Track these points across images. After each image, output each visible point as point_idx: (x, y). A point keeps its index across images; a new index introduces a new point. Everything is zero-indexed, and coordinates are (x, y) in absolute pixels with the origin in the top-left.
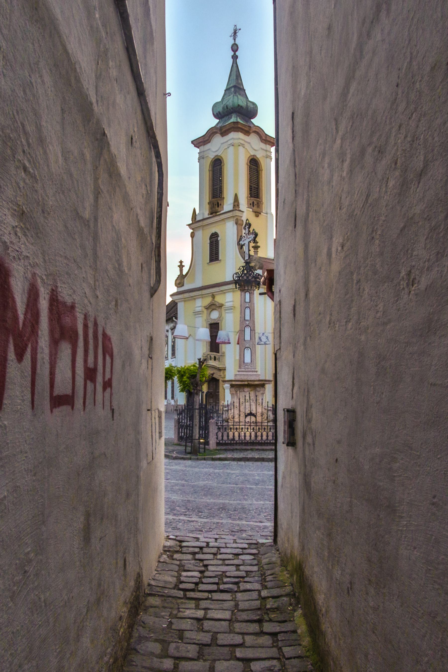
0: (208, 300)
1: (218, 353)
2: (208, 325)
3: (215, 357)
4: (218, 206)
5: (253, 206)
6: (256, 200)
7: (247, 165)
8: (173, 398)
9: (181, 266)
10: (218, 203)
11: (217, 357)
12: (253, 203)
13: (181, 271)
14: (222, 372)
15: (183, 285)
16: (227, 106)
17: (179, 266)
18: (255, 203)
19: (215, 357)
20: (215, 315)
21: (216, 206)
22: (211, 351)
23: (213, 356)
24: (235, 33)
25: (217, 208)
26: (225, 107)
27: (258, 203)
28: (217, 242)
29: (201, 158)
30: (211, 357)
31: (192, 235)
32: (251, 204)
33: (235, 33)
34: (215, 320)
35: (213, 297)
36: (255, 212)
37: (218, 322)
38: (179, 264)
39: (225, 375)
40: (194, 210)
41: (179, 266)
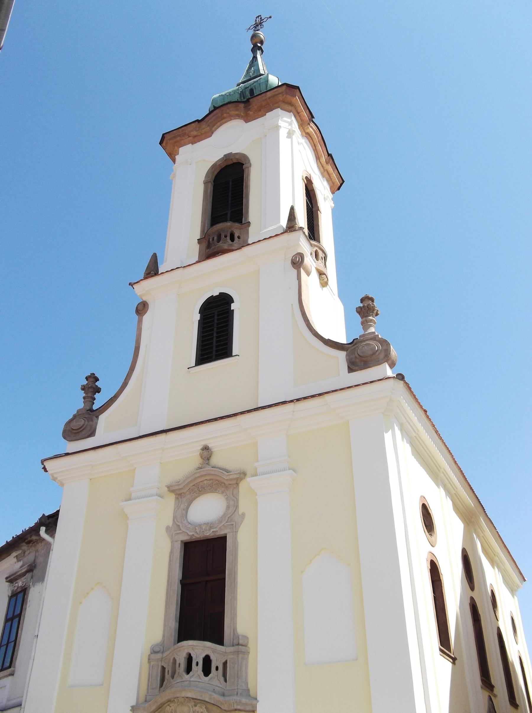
2: (178, 547)
3: (207, 661)
9: (92, 387)
13: (90, 398)
15: (92, 434)
17: (83, 388)
19: (207, 661)
20: (206, 512)
34: (210, 525)
37: (221, 533)
41: (83, 388)
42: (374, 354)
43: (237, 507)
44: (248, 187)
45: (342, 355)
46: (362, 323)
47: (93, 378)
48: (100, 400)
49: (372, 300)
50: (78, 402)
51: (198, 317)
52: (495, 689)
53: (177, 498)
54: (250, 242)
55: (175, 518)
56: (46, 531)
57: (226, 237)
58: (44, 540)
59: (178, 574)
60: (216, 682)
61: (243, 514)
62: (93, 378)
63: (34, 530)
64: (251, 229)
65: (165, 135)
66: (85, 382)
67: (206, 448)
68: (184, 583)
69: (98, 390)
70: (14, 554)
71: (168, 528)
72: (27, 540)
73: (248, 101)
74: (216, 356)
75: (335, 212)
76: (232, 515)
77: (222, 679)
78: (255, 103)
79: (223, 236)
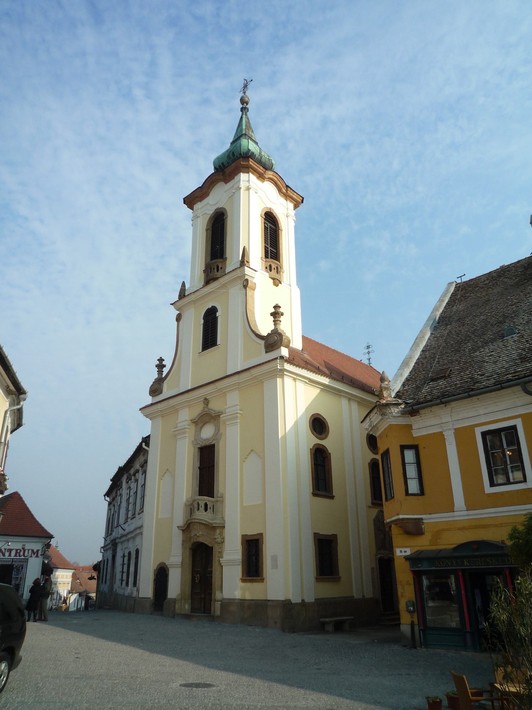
0: (197, 410)
1: (213, 497)
3: (206, 505)
4: (218, 270)
5: (271, 271)
6: (273, 263)
7: (262, 260)
8: (135, 584)
9: (160, 366)
10: (218, 267)
11: (210, 505)
12: (270, 266)
13: (160, 372)
14: (218, 531)
15: (161, 392)
16: (233, 153)
17: (157, 366)
18: (273, 266)
19: (206, 505)
20: (207, 433)
21: (216, 270)
22: (201, 494)
23: (202, 504)
24: (245, 86)
25: (216, 273)
26: (231, 155)
27: (277, 268)
28: (215, 319)
29: (195, 218)
30: (198, 504)
31: (179, 318)
32: (266, 268)
33: (245, 86)
34: (207, 440)
35: (206, 401)
36: (273, 279)
37: (213, 443)
38: (158, 362)
39: (223, 538)
40: (183, 284)
41: (157, 366)
42: (275, 342)
43: (219, 430)
44: (226, 232)
45: (262, 342)
46: (274, 321)
47: (161, 360)
48: (165, 371)
51: (202, 321)
54: (227, 270)
56: (146, 445)
57: (214, 269)
58: (144, 449)
59: (198, 464)
60: (209, 515)
61: (222, 433)
62: (161, 360)
63: (141, 444)
64: (228, 262)
66: (158, 362)
68: (213, 466)
69: (165, 366)
70: (142, 454)
71: (192, 441)
74: (211, 345)
76: (217, 433)
77: (212, 513)
78: (228, 171)
79: (212, 269)
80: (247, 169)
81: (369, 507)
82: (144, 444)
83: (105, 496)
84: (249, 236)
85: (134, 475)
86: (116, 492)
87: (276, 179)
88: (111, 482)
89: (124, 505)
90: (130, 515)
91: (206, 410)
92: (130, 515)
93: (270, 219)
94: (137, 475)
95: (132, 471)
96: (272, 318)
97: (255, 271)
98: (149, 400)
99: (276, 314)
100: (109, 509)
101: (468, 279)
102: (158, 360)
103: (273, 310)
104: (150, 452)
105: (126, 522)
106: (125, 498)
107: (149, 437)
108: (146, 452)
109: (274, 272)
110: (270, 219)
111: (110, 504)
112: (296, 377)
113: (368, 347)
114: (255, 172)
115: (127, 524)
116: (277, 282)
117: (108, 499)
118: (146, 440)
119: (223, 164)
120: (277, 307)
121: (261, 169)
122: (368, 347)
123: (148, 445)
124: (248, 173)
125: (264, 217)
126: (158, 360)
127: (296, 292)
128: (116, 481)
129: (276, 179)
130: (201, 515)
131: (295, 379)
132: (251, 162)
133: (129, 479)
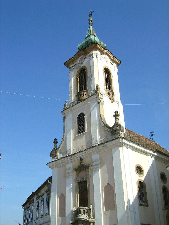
0: (77, 163)
2: (77, 183)
4: (84, 96)
5: (109, 95)
9: (55, 142)
10: (84, 94)
12: (109, 93)
13: (56, 146)
18: (110, 93)
32: (107, 94)
36: (111, 99)
37: (86, 180)
46: (115, 119)
47: (55, 139)
48: (58, 145)
49: (118, 112)
50: (52, 147)
52: (83, 161)
53: (76, 172)
55: (76, 178)
62: (55, 139)
63: (47, 181)
65: (66, 63)
66: (54, 141)
67: (81, 158)
69: (57, 142)
72: (46, 183)
73: (65, 109)
75: (119, 74)
80: (96, 49)
81: (164, 210)
82: (49, 181)
83: (22, 206)
84: (98, 80)
85: (42, 196)
86: (30, 205)
87: (108, 53)
88: (27, 199)
89: (35, 210)
90: (40, 215)
91: (81, 163)
92: (40, 215)
93: (107, 71)
94: (43, 196)
95: (40, 194)
96: (114, 118)
97: (102, 95)
98: (50, 159)
99: (116, 115)
100: (25, 212)
101: (122, 104)
102: (54, 139)
103: (54, 141)
104: (52, 185)
105: (37, 218)
106: (36, 207)
107: (51, 178)
108: (50, 185)
109: (111, 96)
110: (107, 71)
111: (25, 210)
112: (128, 146)
113: (152, 133)
114: (99, 50)
115: (38, 220)
116: (112, 100)
117: (24, 207)
118: (50, 179)
119: (82, 47)
120: (116, 112)
121: (102, 49)
122: (152, 133)
123: (51, 181)
124: (96, 50)
125: (104, 70)
126: (54, 139)
127: (121, 105)
128: (30, 199)
129: (108, 53)
130: (84, 216)
131: (127, 148)
132: (98, 46)
133: (38, 198)
